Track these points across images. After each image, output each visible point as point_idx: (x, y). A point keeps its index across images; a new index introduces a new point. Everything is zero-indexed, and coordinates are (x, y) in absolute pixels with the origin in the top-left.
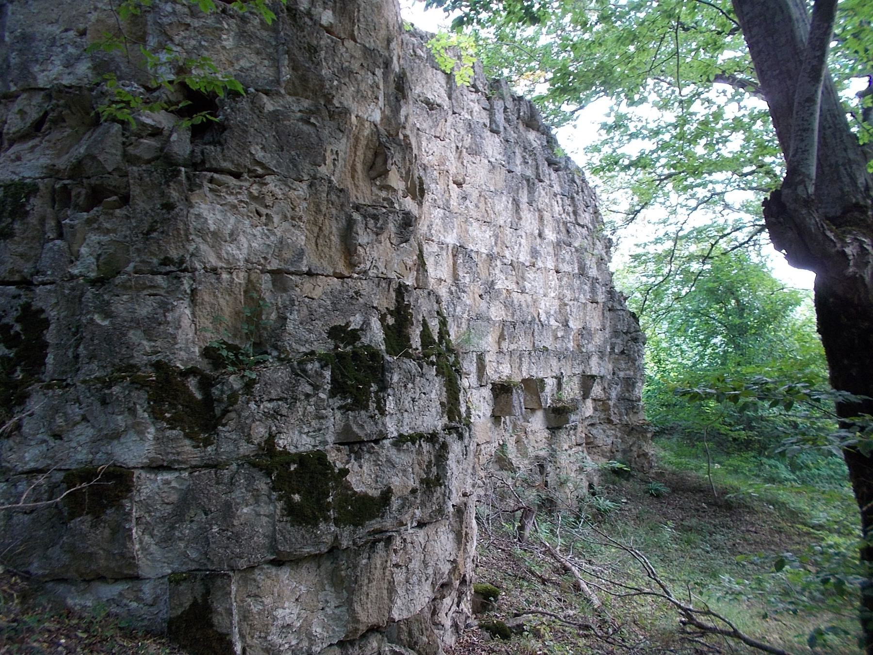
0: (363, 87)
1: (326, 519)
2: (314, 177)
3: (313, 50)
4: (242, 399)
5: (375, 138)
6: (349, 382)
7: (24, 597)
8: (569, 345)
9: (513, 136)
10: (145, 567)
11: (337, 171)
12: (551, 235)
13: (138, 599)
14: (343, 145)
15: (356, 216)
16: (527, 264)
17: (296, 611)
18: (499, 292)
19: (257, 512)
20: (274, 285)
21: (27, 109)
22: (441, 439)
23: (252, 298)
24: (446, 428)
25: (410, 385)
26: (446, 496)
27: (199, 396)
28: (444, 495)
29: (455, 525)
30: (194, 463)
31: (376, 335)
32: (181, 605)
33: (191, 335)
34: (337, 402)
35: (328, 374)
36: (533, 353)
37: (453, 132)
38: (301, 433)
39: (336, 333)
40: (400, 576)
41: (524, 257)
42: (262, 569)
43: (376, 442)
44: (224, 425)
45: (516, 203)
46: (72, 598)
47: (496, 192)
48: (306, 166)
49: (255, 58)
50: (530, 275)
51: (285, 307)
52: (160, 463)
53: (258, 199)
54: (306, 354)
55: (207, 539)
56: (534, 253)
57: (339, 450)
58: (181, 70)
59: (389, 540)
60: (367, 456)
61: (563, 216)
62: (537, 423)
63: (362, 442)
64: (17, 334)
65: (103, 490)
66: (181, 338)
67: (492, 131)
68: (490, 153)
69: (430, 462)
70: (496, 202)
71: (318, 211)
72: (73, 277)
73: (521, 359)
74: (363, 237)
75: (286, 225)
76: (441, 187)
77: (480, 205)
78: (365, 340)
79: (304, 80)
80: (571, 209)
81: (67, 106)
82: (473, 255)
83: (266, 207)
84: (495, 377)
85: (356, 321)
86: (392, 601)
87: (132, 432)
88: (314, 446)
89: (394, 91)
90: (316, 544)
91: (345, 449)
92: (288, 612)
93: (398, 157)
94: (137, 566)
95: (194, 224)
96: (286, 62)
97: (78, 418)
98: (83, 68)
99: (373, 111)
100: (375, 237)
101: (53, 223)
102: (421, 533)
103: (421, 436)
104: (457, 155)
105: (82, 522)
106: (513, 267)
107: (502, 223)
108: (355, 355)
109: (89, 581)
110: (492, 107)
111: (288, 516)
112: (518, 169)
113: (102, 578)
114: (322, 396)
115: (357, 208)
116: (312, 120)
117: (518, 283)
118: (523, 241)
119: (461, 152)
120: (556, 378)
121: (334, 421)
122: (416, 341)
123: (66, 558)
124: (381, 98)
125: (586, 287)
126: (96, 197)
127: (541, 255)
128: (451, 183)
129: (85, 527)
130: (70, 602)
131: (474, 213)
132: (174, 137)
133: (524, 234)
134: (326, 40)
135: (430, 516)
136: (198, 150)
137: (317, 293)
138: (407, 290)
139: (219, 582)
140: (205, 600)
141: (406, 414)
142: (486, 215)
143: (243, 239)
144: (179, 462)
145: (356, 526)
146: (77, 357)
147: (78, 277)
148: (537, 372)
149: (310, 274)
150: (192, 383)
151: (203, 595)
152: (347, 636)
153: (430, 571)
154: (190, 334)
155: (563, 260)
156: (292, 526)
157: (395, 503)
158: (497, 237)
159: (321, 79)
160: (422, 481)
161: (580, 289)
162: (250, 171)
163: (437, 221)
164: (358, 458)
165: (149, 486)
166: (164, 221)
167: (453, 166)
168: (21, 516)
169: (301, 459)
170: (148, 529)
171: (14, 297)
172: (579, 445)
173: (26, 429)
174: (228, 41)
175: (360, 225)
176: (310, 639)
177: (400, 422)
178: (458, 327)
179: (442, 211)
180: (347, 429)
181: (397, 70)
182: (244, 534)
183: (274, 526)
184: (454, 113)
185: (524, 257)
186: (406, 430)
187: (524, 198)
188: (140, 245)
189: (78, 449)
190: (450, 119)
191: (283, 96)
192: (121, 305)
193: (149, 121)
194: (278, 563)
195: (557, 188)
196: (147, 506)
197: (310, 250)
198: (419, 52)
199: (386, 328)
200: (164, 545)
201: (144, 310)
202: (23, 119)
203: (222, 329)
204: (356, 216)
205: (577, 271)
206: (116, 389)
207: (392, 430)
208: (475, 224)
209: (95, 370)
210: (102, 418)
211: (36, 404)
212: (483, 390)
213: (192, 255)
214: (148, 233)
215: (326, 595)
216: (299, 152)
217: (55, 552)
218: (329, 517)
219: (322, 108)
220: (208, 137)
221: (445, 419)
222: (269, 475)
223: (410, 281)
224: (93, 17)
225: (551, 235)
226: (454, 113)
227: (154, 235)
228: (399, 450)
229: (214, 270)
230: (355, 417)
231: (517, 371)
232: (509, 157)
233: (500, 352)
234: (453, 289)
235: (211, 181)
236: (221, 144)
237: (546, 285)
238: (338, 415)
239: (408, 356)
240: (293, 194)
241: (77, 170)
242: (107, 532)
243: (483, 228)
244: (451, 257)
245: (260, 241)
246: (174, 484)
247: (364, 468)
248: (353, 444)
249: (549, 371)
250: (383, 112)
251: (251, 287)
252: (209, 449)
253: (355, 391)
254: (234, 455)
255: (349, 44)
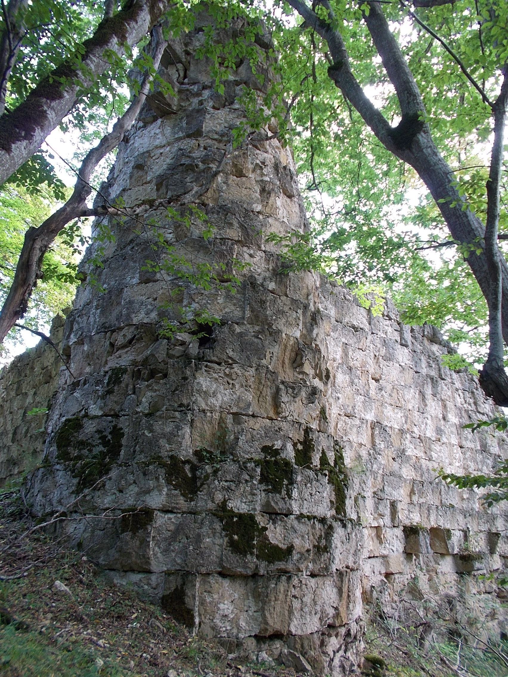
0: (290, 319)
1: (252, 554)
2: (259, 365)
3: (263, 302)
4: (211, 478)
5: (296, 345)
6: (271, 476)
7: (95, 574)
8: (474, 506)
9: (418, 348)
10: (154, 566)
11: (272, 363)
12: (453, 419)
13: (149, 584)
14: (276, 349)
15: (282, 386)
16: (434, 439)
17: (231, 608)
18: (409, 458)
19: (214, 543)
20: (234, 421)
21: (127, 334)
22: (328, 523)
23: (222, 427)
24: (334, 518)
25: (309, 485)
26: (331, 560)
27: (190, 475)
28: (330, 559)
29: (337, 582)
30: (184, 510)
31: (290, 453)
32: (170, 589)
33: (189, 443)
34: (263, 487)
35: (259, 470)
36: (440, 507)
37: (372, 346)
38: (241, 501)
39: (266, 449)
40: (296, 604)
41: (430, 433)
42: (214, 576)
43: (286, 516)
44: (201, 491)
45: (422, 395)
46: (117, 579)
47: (405, 386)
48: (255, 360)
49: (233, 308)
50: (436, 447)
51: (239, 433)
52: (167, 508)
53: (229, 376)
54: (248, 459)
55: (187, 552)
56: (439, 431)
57: (263, 516)
58: (198, 315)
59: (289, 578)
60: (280, 523)
61: (465, 406)
62: (447, 566)
63: (277, 514)
64: (109, 440)
65: (138, 520)
66: (184, 444)
67: (402, 345)
68: (400, 359)
69: (321, 536)
70: (406, 393)
71: (260, 383)
72: (137, 413)
73: (428, 511)
74: (285, 398)
75: (242, 389)
76: (363, 381)
77: (393, 395)
78: (283, 455)
79: (257, 317)
80: (472, 401)
81: (145, 332)
82: (387, 429)
83: (233, 380)
84: (407, 523)
85: (278, 444)
86: (290, 619)
87: (156, 490)
88: (249, 511)
89: (311, 321)
90: (245, 567)
91: (267, 516)
92: (226, 607)
93: (310, 356)
94: (150, 564)
95: (196, 387)
96: (248, 309)
97: (132, 482)
98: (154, 315)
99: (295, 331)
100: (292, 399)
101: (132, 387)
102: (312, 582)
103: (315, 517)
104: (376, 361)
105: (127, 535)
106: (421, 440)
107: (411, 408)
108: (276, 463)
109: (126, 571)
110: (401, 329)
111: (230, 547)
112: (424, 371)
113: (133, 571)
114: (255, 482)
115: (283, 383)
116: (260, 336)
117: (426, 453)
118: (429, 422)
119: (378, 359)
120: (463, 531)
121: (260, 497)
122: (316, 461)
123: (117, 556)
124: (301, 324)
125: (488, 461)
126: (152, 374)
127: (445, 433)
128: (370, 379)
129: (128, 538)
130: (115, 581)
131: (388, 400)
132: (191, 345)
133: (429, 417)
134: (270, 296)
135: (319, 570)
136: (201, 351)
137: (257, 426)
138: (311, 431)
139: (190, 578)
140: (182, 588)
141: (305, 502)
142: (398, 402)
143: (219, 396)
144: (177, 509)
145: (269, 562)
146: (134, 451)
147: (140, 413)
148: (444, 523)
149: (253, 416)
150: (187, 467)
151: (181, 585)
152: (260, 632)
153: (318, 608)
154: (189, 443)
155: (466, 439)
156: (232, 553)
157: (296, 557)
158: (407, 417)
159: (266, 316)
160: (314, 546)
161: (483, 462)
162: (225, 362)
163: (359, 404)
164: (274, 523)
165: (161, 520)
166: (183, 385)
167: (372, 368)
168: (99, 531)
169: (241, 516)
170: (157, 544)
171: (110, 422)
172: (489, 593)
173: (107, 487)
174: (221, 300)
175: (283, 391)
176: (238, 629)
177: (301, 506)
178: (374, 479)
179: (363, 397)
180: (267, 504)
181: (313, 310)
182: (205, 553)
183: (222, 551)
184: (373, 333)
185: (430, 433)
186: (305, 512)
187: (429, 391)
188: (170, 397)
189: (130, 499)
190: (370, 337)
191: (245, 325)
192: (158, 427)
193: (180, 338)
194: (223, 575)
195: (458, 385)
196: (159, 531)
197: (254, 404)
198: (348, 297)
199: (297, 451)
200: (164, 553)
201: (168, 429)
202: (124, 338)
203: (204, 442)
204: (282, 386)
205: (479, 448)
206: (151, 467)
207: (296, 508)
208: (389, 408)
209: (142, 458)
210: (143, 482)
211: (114, 474)
212: (395, 530)
213: (194, 403)
214: (174, 391)
215: (249, 603)
216: (252, 351)
217: (112, 552)
218: (253, 553)
219: (266, 330)
220: (207, 345)
221: (333, 512)
222: (221, 521)
223: (314, 426)
224: (160, 292)
225: (453, 419)
226: (373, 333)
227: (177, 392)
228: (299, 522)
229: (204, 411)
230: (273, 497)
231: (426, 520)
232: (416, 362)
233: (411, 503)
234: (371, 452)
235: (206, 366)
236: (213, 349)
237: (451, 455)
238: (263, 494)
239: (310, 469)
240: (247, 374)
241: (145, 362)
242: (138, 543)
243: (396, 411)
244: (370, 429)
245: (228, 397)
246: (173, 520)
247: (277, 529)
248: (273, 514)
249: (456, 525)
250: (301, 332)
251: (221, 421)
252: (192, 503)
253: (273, 482)
254: (204, 508)
255: (284, 298)
